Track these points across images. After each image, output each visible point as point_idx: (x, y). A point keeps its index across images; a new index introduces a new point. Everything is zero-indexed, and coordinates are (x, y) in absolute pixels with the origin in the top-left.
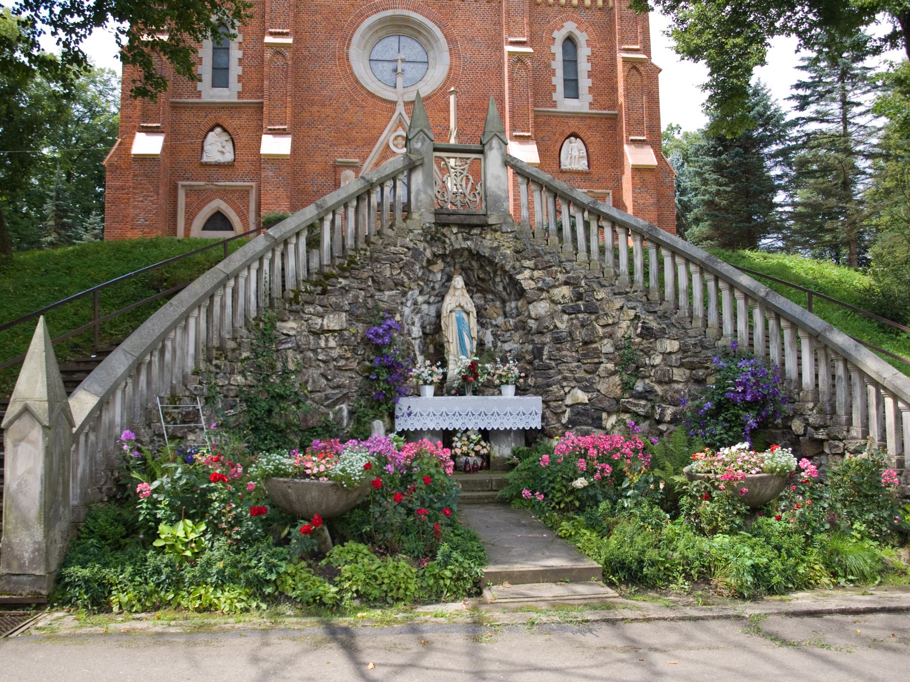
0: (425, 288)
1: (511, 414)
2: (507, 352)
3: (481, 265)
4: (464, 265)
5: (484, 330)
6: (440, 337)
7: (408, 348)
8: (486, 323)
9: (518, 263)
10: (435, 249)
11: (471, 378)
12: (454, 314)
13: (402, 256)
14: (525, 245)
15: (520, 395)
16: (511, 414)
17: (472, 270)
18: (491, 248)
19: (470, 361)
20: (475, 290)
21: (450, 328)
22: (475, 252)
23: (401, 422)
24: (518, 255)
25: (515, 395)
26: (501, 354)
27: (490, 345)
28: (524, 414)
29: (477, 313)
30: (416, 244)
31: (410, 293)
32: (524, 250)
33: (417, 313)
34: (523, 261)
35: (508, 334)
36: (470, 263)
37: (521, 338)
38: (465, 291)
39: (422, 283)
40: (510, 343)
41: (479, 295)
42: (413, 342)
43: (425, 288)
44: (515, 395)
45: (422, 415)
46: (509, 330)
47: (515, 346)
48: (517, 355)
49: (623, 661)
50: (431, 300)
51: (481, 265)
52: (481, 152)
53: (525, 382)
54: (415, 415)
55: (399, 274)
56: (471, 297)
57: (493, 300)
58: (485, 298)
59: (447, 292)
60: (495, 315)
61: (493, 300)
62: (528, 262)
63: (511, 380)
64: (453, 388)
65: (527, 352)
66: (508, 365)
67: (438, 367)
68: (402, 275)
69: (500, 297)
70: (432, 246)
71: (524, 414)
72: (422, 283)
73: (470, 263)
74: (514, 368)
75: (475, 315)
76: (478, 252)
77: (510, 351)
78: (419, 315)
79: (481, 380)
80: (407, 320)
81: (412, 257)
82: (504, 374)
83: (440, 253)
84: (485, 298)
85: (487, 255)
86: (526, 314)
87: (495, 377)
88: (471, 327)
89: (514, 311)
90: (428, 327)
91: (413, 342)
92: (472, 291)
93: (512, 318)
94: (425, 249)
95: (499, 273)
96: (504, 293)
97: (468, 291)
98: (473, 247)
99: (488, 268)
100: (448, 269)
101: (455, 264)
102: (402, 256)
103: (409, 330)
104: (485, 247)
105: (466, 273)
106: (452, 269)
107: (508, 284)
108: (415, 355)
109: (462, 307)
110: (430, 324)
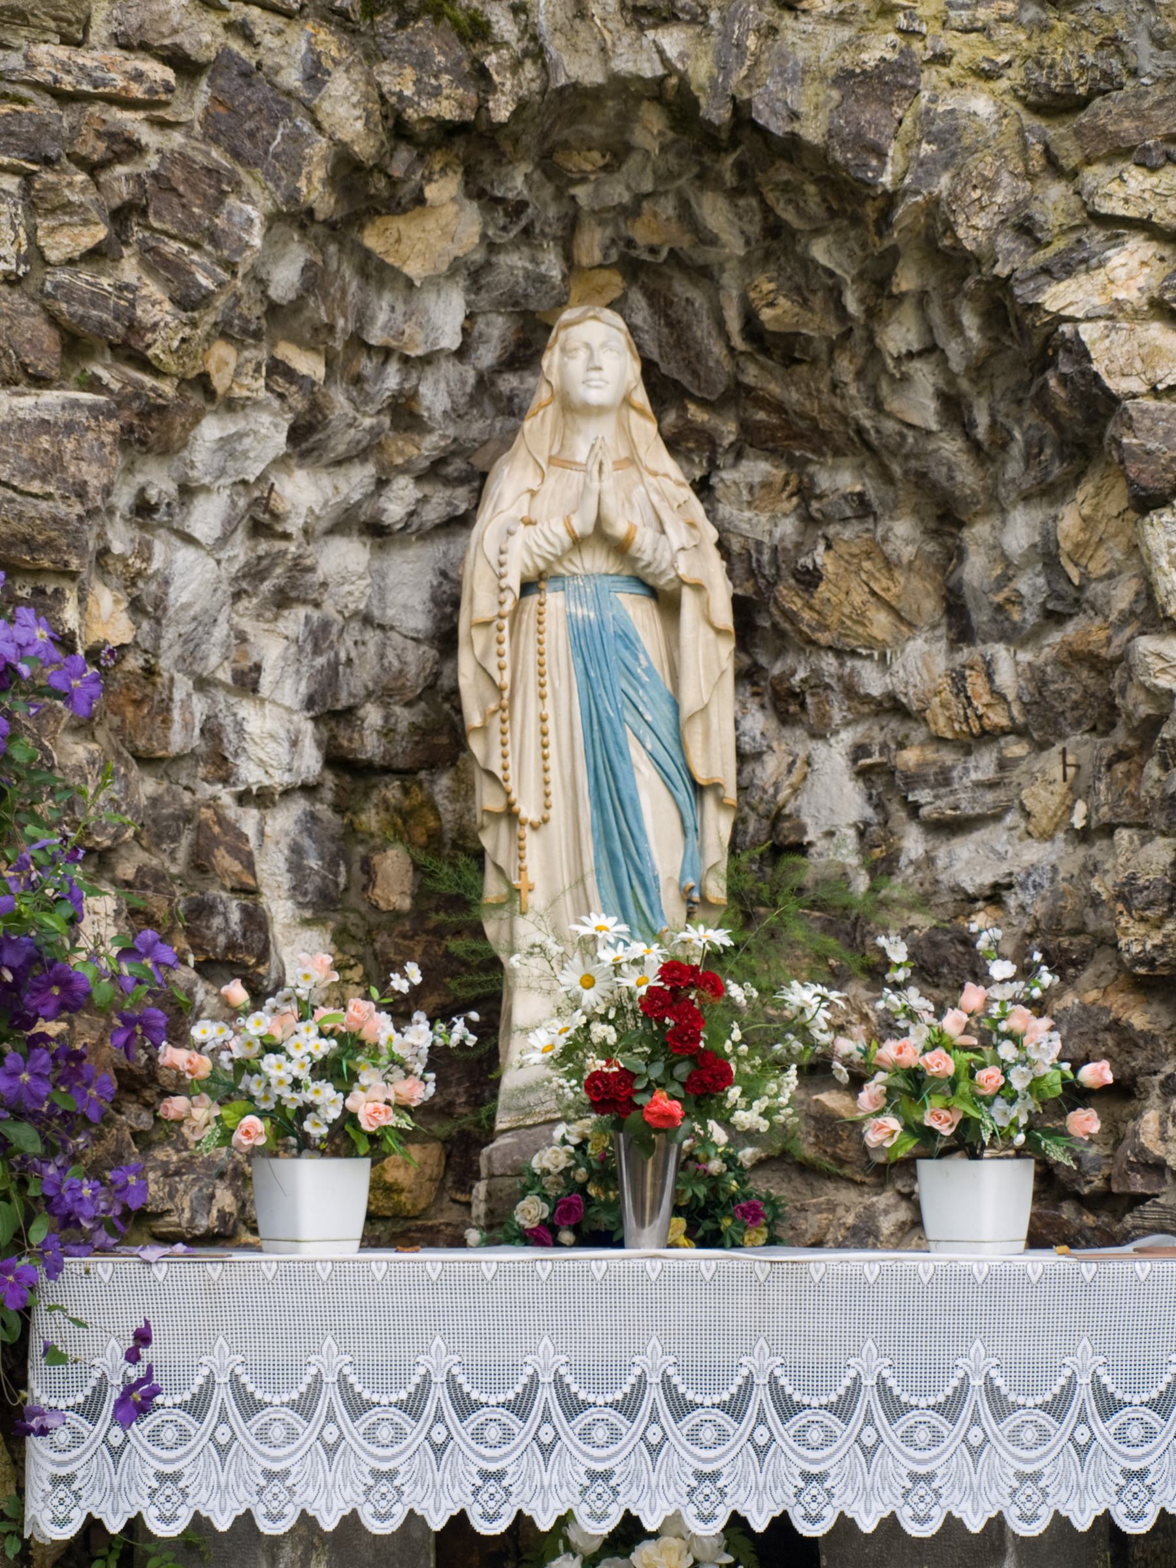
0: (340, 401)
1: (1001, 1407)
2: (968, 901)
3: (774, 230)
4: (642, 233)
5: (798, 742)
6: (464, 791)
7: (200, 865)
8: (817, 683)
9: (1056, 192)
10: (389, 83)
11: (664, 1102)
12: (554, 600)
13: (132, 122)
14: (1112, 43)
15: (1073, 1240)
16: (1001, 1407)
17: (704, 274)
18: (845, 78)
19: (655, 956)
20: (729, 431)
21: (527, 709)
22: (717, 113)
23: (78, 1463)
24: (1056, 131)
25: (1036, 1240)
26: (923, 922)
27: (848, 854)
28: (1109, 1406)
29: (740, 606)
30: (243, 30)
31: (211, 429)
32: (1106, 85)
33: (282, 600)
34: (1096, 176)
35: (983, 765)
36: (687, 215)
37: (1075, 791)
38: (645, 430)
39: (309, 365)
40: (995, 836)
41: (757, 469)
42: (248, 820)
43: (340, 401)
44: (1036, 1240)
45: (250, 1406)
46: (988, 736)
47: (1035, 853)
48: (1053, 924)
49: (619, 329)
50: (394, 509)
51: (774, 230)
52: (893, 773)
53: (1114, 1134)
54: (197, 1407)
55: (96, 255)
56: (703, 488)
57: (863, 508)
58: (805, 493)
59: (507, 441)
60: (880, 623)
61: (863, 508)
62: (1137, 180)
63: (999, 1115)
64: (533, 1182)
65: (1126, 894)
66: (973, 995)
67: (400, 1011)
68: (129, 269)
69: (921, 479)
70: (373, 56)
71: (1109, 1406)
72: (309, 365)
73: (687, 215)
74: (1019, 1019)
75: (724, 616)
76: (741, 113)
77: (995, 896)
78: (295, 621)
79: (746, 1118)
80: (192, 649)
81: (213, 130)
82: (940, 1064)
83: (447, 110)
84: (805, 493)
85: (812, 132)
86: (1123, 595)
87: (872, 1091)
88: (690, 701)
89: (1030, 584)
90: (373, 715)
91: (248, 820)
92: (708, 441)
93: (1013, 636)
94: (315, 75)
95: (906, 280)
96: (951, 447)
97: (673, 444)
98: (701, 71)
99: (820, 251)
100: (514, 262)
101: (572, 223)
102: (132, 122)
103: (211, 731)
104: (799, 75)
105: (660, 303)
106: (552, 265)
107: (979, 370)
108: (256, 920)
109: (620, 548)
110: (384, 694)
